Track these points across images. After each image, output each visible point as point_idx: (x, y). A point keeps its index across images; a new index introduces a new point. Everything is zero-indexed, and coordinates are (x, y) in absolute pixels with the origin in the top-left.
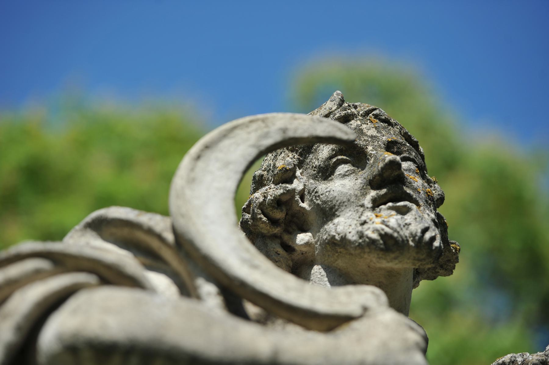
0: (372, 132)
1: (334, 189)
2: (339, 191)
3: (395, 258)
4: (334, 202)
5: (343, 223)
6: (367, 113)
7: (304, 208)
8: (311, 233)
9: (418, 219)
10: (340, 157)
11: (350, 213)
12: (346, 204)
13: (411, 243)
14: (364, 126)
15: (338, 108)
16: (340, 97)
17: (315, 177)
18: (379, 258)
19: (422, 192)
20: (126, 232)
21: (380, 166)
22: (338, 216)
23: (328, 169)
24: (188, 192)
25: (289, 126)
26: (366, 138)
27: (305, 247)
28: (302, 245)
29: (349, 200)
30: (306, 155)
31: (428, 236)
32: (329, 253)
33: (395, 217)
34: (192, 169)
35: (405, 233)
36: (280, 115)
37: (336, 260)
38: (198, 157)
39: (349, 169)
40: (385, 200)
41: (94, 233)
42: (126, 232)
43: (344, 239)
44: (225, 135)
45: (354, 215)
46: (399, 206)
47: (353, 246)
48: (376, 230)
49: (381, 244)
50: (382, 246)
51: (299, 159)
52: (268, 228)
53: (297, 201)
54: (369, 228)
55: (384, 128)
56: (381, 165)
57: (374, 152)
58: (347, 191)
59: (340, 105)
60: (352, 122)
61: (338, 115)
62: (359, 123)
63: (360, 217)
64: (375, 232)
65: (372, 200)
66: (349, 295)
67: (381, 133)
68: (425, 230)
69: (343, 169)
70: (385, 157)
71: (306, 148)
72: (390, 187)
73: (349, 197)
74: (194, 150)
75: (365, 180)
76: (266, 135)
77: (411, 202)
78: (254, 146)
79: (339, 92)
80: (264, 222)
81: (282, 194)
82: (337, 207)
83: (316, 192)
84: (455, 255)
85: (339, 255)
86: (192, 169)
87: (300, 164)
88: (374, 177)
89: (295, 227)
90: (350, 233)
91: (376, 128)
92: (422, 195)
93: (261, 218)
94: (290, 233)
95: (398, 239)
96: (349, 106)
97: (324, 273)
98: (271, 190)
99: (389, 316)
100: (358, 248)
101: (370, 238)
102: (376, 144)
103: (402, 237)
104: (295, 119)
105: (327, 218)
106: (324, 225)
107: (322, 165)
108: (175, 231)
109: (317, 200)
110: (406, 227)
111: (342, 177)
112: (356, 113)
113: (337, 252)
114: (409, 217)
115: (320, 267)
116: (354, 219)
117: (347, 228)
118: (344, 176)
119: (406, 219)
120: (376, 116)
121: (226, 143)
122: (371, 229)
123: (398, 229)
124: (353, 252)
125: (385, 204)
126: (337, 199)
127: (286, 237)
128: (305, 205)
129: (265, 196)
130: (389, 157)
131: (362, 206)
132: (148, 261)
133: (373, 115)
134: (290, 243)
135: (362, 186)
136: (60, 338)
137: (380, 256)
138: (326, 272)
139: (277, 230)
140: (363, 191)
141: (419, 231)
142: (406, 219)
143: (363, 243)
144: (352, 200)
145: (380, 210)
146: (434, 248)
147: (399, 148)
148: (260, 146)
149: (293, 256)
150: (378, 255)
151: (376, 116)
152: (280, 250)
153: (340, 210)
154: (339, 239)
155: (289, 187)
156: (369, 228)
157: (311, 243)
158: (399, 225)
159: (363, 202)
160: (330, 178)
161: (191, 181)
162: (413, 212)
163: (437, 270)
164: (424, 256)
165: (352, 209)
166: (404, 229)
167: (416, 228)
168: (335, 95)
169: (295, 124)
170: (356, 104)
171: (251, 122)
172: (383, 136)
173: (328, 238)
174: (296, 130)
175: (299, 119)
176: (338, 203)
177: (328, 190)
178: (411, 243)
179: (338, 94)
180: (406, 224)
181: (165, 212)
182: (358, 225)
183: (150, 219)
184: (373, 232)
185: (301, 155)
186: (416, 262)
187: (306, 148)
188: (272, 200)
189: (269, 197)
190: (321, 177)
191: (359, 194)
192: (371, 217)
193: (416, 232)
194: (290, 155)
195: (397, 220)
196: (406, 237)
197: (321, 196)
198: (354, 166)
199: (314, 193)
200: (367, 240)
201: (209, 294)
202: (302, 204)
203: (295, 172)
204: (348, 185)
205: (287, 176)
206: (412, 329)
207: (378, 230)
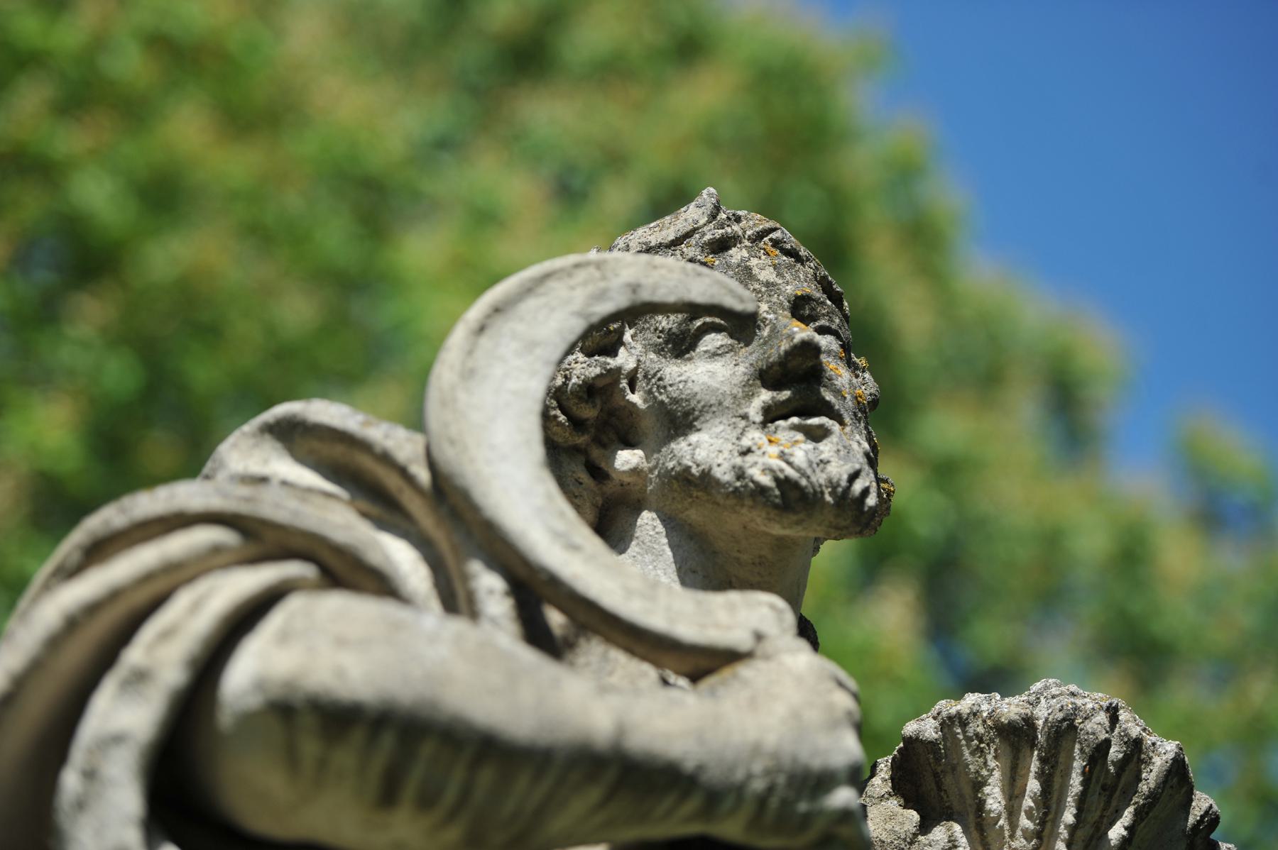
0: (768, 275)
1: (694, 378)
3: (798, 523)
4: (693, 403)
5: (706, 445)
6: (760, 236)
7: (634, 405)
11: (721, 427)
13: (828, 498)
14: (754, 262)
15: (709, 222)
16: (713, 200)
17: (659, 350)
18: (769, 520)
19: (849, 397)
20: (338, 451)
21: (783, 348)
22: (699, 430)
23: (684, 338)
24: (462, 396)
25: (644, 281)
26: (757, 286)
28: (624, 472)
29: (720, 404)
31: (858, 487)
32: (676, 495)
33: (803, 446)
34: (470, 353)
35: (820, 478)
38: (481, 329)
40: (785, 411)
41: (278, 445)
43: (706, 476)
44: (529, 290)
46: (810, 426)
48: (767, 470)
50: (777, 501)
53: (623, 390)
54: (756, 463)
55: (790, 267)
56: (785, 346)
57: (771, 316)
59: (713, 217)
60: (733, 251)
61: (708, 237)
62: (745, 253)
63: (738, 439)
66: (732, 608)
67: (783, 277)
68: (854, 476)
70: (794, 333)
72: (795, 387)
73: (720, 397)
76: (601, 296)
78: (579, 314)
79: (712, 190)
80: (560, 424)
81: (598, 376)
82: (697, 413)
83: (660, 379)
86: (470, 353)
88: (770, 366)
92: (850, 403)
93: (556, 417)
94: (604, 446)
96: (728, 218)
97: (660, 528)
98: (578, 366)
99: (801, 658)
101: (756, 483)
102: (774, 299)
103: (813, 487)
104: (655, 267)
105: (676, 429)
106: (669, 442)
107: (674, 330)
108: (432, 465)
109: (661, 394)
112: (740, 233)
113: (691, 496)
114: (827, 448)
115: (655, 516)
116: (727, 439)
117: (713, 455)
118: (714, 355)
119: (822, 452)
120: (776, 243)
121: (531, 303)
122: (760, 466)
123: (809, 472)
124: (722, 502)
125: (785, 417)
126: (698, 397)
127: (596, 453)
128: (636, 398)
129: (566, 377)
130: (802, 332)
131: (745, 417)
132: (375, 510)
134: (603, 465)
136: (260, 685)
137: (772, 515)
138: (665, 526)
139: (581, 440)
141: (845, 477)
142: (822, 452)
144: (726, 404)
145: (776, 428)
150: (768, 513)
151: (776, 243)
152: (584, 477)
155: (612, 363)
156: (756, 463)
157: (642, 470)
161: (468, 374)
162: (834, 438)
164: (848, 522)
166: (818, 470)
167: (838, 470)
170: (740, 213)
171: (577, 266)
172: (788, 283)
173: (678, 469)
174: (655, 288)
175: (662, 266)
176: (700, 406)
177: (683, 378)
178: (828, 498)
179: (710, 195)
181: (417, 422)
182: (736, 454)
183: (387, 436)
189: (574, 380)
190: (671, 351)
191: (740, 395)
192: (760, 442)
193: (839, 479)
195: (806, 452)
196: (820, 486)
197: (669, 389)
199: (656, 379)
200: (751, 485)
206: (841, 684)
207: (772, 470)
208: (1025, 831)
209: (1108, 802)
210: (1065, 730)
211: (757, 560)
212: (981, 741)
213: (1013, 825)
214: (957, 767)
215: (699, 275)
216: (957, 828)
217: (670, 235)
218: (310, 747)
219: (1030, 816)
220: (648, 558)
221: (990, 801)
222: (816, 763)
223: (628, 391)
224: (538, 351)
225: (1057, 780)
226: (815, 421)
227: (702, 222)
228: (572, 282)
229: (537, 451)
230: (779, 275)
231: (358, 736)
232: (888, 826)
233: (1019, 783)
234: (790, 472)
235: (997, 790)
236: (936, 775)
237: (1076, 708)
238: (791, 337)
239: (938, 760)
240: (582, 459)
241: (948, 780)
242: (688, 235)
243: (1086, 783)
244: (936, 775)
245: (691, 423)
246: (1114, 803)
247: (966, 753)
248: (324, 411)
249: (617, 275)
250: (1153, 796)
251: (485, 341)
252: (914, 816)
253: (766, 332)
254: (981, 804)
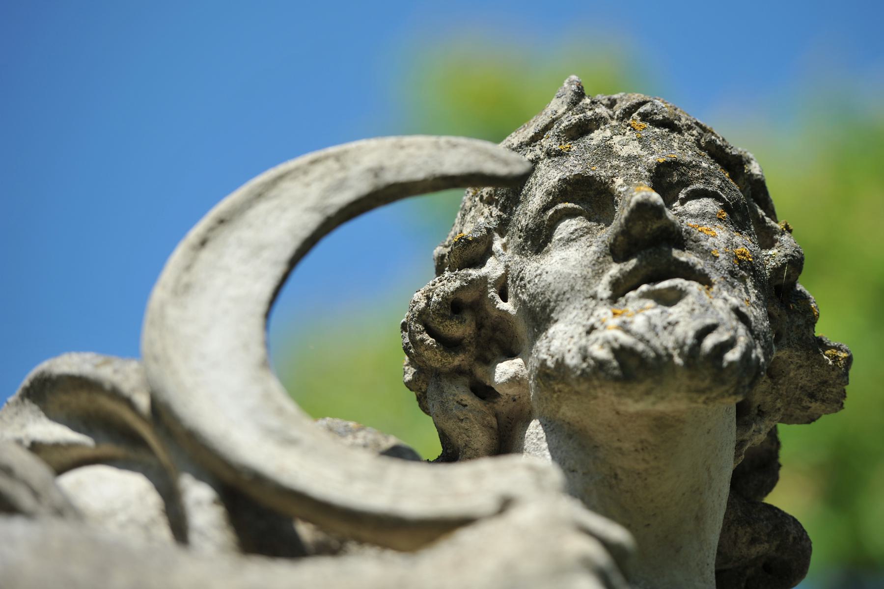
0: (633, 148)
1: (547, 269)
2: (556, 272)
3: (648, 393)
6: (628, 113)
7: (506, 312)
8: (522, 358)
9: (697, 312)
10: (560, 206)
11: (575, 312)
12: (568, 296)
13: (678, 360)
14: (617, 139)
16: (574, 87)
19: (722, 256)
22: (556, 321)
23: (541, 231)
24: (172, 312)
25: (387, 163)
27: (510, 387)
29: (572, 289)
30: (512, 209)
31: (709, 342)
34: (188, 268)
35: (666, 341)
36: (373, 143)
37: (559, 407)
38: (203, 243)
39: (578, 227)
40: (635, 280)
41: (35, 407)
42: (82, 399)
43: (560, 364)
44: (259, 196)
45: (581, 315)
46: (660, 290)
47: (573, 376)
49: (615, 368)
50: (617, 372)
51: (499, 217)
52: (439, 356)
53: (493, 299)
58: (570, 271)
59: (574, 103)
61: (566, 123)
63: (588, 319)
64: (606, 345)
65: (610, 282)
66: (478, 477)
71: (511, 195)
72: (650, 253)
75: (603, 246)
76: (340, 186)
77: (687, 279)
78: (314, 209)
80: (429, 347)
82: (552, 304)
84: (833, 370)
85: (558, 396)
87: (503, 227)
89: (495, 350)
90: (569, 351)
91: (640, 140)
93: (422, 340)
95: (644, 355)
97: (542, 434)
100: (581, 380)
103: (654, 349)
105: (539, 326)
110: (670, 328)
111: (564, 245)
113: (554, 392)
116: (579, 323)
118: (568, 241)
119: (671, 314)
120: (645, 117)
121: (262, 208)
122: (600, 342)
123: (648, 336)
124: (577, 388)
125: (635, 288)
126: (552, 288)
127: (479, 371)
128: (508, 306)
131: (594, 297)
133: (639, 114)
135: (596, 256)
139: (458, 360)
140: (597, 268)
141: (691, 333)
142: (671, 314)
143: (588, 370)
144: (577, 288)
145: (626, 301)
146: (725, 364)
147: (683, 174)
148: (327, 207)
149: (495, 405)
151: (645, 117)
152: (468, 398)
153: (558, 308)
154: (552, 366)
157: (522, 379)
158: (653, 327)
159: (595, 289)
160: (546, 249)
161: (183, 290)
162: (690, 299)
163: (804, 404)
165: (578, 306)
168: (566, 85)
169: (402, 155)
170: (615, 96)
171: (314, 162)
174: (400, 168)
176: (554, 296)
177: (539, 272)
178: (678, 360)
179: (571, 83)
180: (669, 323)
184: (602, 346)
185: (504, 209)
186: (695, 395)
187: (511, 195)
188: (439, 303)
189: (435, 298)
194: (486, 211)
198: (590, 220)
201: (199, 503)
202: (502, 305)
203: (491, 243)
204: (572, 260)
205: (472, 252)
211: (639, 446)
215: (455, 146)
217: (530, 132)
223: (498, 299)
224: (266, 254)
227: (560, 112)
228: (308, 179)
240: (467, 380)
242: (547, 128)
245: (549, 315)
248: (70, 363)
249: (357, 163)
251: (206, 255)
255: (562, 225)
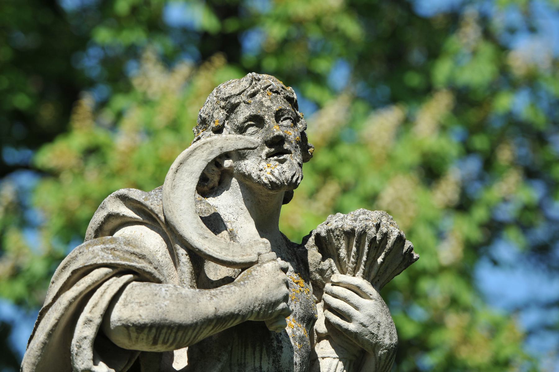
6: (265, 88)
10: (249, 123)
11: (254, 159)
13: (286, 184)
14: (264, 99)
19: (293, 142)
24: (172, 195)
25: (224, 146)
31: (294, 179)
43: (250, 175)
44: (190, 155)
56: (272, 136)
61: (249, 93)
69: (251, 130)
74: (174, 166)
76: (211, 153)
97: (238, 185)
108: (165, 216)
118: (251, 134)
120: (271, 90)
121: (191, 158)
131: (261, 157)
151: (271, 90)
161: (173, 187)
162: (288, 162)
178: (286, 184)
179: (250, 76)
185: (227, 112)
190: (239, 132)
208: (352, 262)
209: (377, 251)
210: (363, 233)
212: (338, 236)
213: (349, 260)
214: (331, 243)
216: (332, 261)
218: (134, 335)
219: (353, 258)
220: (235, 194)
221: (341, 254)
222: (273, 299)
225: (361, 248)
226: (282, 158)
227: (247, 86)
228: (203, 150)
229: (199, 175)
230: (272, 102)
231: (146, 331)
232: (313, 258)
233: (350, 247)
234: (274, 179)
235: (344, 250)
236: (326, 245)
237: (366, 226)
238: (273, 132)
239: (326, 241)
241: (329, 247)
243: (369, 249)
244: (326, 245)
246: (379, 251)
247: (334, 240)
250: (390, 249)
252: (320, 256)
253: (267, 126)
254: (339, 255)
255: (250, 129)
